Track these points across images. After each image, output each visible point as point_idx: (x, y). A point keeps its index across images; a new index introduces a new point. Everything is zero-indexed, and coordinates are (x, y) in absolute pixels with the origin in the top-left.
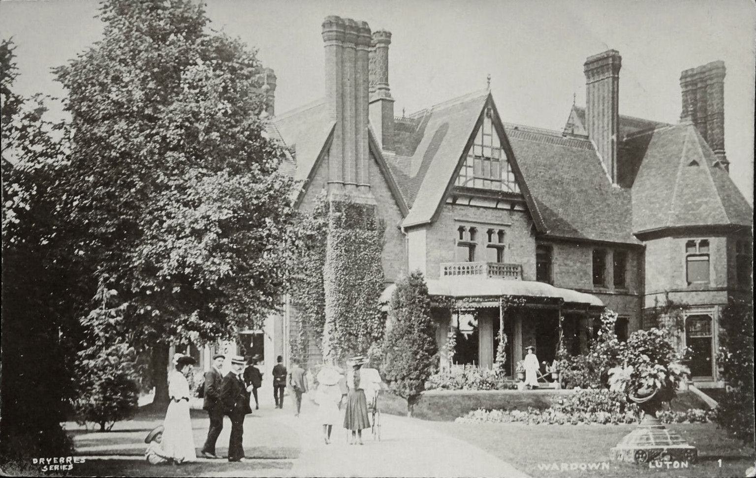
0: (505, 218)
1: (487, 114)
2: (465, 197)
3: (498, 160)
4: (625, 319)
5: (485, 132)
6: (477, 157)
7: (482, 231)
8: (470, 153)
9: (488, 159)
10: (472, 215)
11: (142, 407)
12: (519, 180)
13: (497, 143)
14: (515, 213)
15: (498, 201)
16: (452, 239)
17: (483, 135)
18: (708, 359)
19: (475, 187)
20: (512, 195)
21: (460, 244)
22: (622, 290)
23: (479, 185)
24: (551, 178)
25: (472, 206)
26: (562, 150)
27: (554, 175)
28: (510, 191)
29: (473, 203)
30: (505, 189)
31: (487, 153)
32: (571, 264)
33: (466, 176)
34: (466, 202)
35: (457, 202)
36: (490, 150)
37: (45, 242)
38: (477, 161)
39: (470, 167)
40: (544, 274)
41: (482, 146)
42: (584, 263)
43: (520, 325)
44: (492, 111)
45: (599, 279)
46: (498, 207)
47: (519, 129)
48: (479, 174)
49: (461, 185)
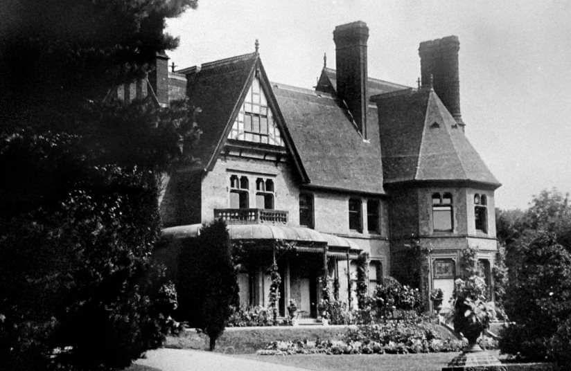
0: (271, 169)
1: (256, 76)
2: (235, 150)
3: (266, 117)
4: (379, 261)
5: (254, 92)
6: (247, 113)
7: (252, 180)
8: (242, 109)
9: (257, 115)
10: (242, 165)
11: (338, 65)
12: (285, 134)
13: (264, 102)
14: (230, 158)
15: (266, 154)
16: (225, 187)
17: (252, 94)
18: (297, 255)
19: (254, 141)
20: (279, 148)
21: (233, 191)
22: (376, 235)
23: (249, 138)
24: (308, 133)
25: (267, 160)
26: (318, 107)
27: (312, 129)
28: (277, 144)
29: (267, 158)
30: (272, 143)
31: (256, 110)
32: (330, 210)
33: (238, 130)
34: (238, 154)
35: (231, 153)
36: (258, 107)
37: (2, 329)
38: (246, 116)
39: (241, 122)
40: (307, 218)
41: (252, 104)
42: (341, 209)
43: (288, 272)
44: (260, 73)
45: (355, 223)
46: (242, 155)
47: (279, 87)
48: (249, 129)
49: (234, 138)
